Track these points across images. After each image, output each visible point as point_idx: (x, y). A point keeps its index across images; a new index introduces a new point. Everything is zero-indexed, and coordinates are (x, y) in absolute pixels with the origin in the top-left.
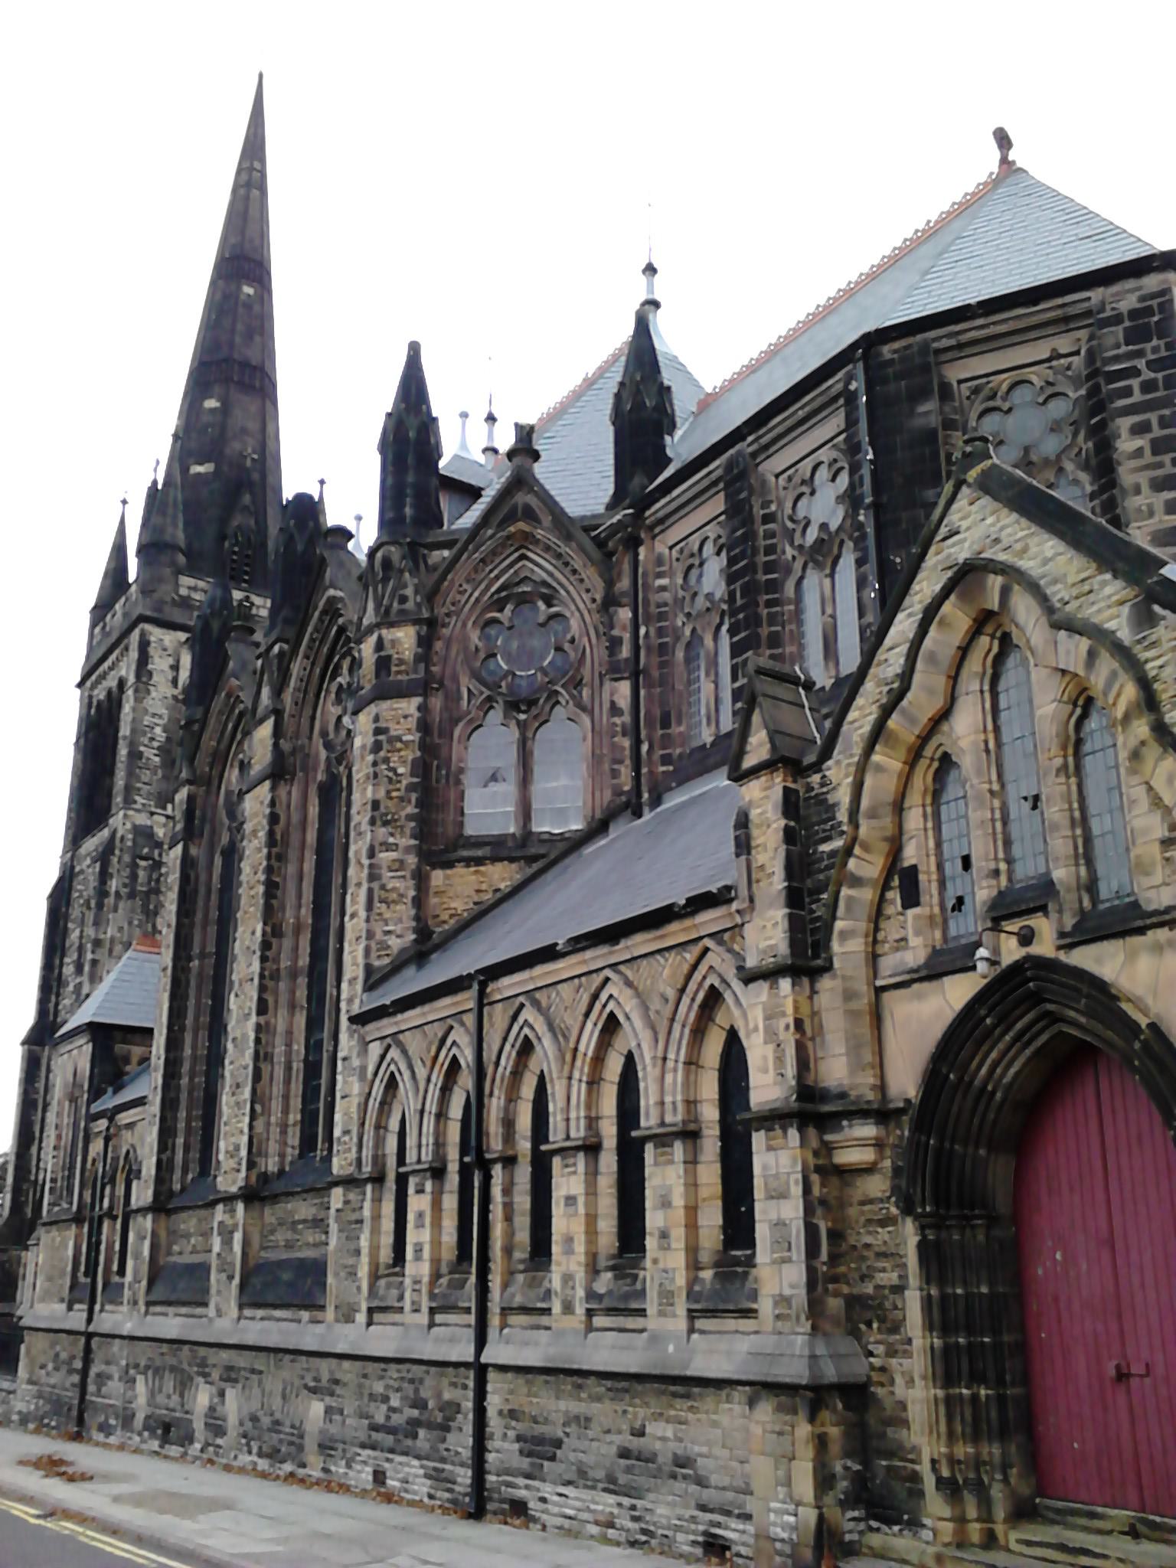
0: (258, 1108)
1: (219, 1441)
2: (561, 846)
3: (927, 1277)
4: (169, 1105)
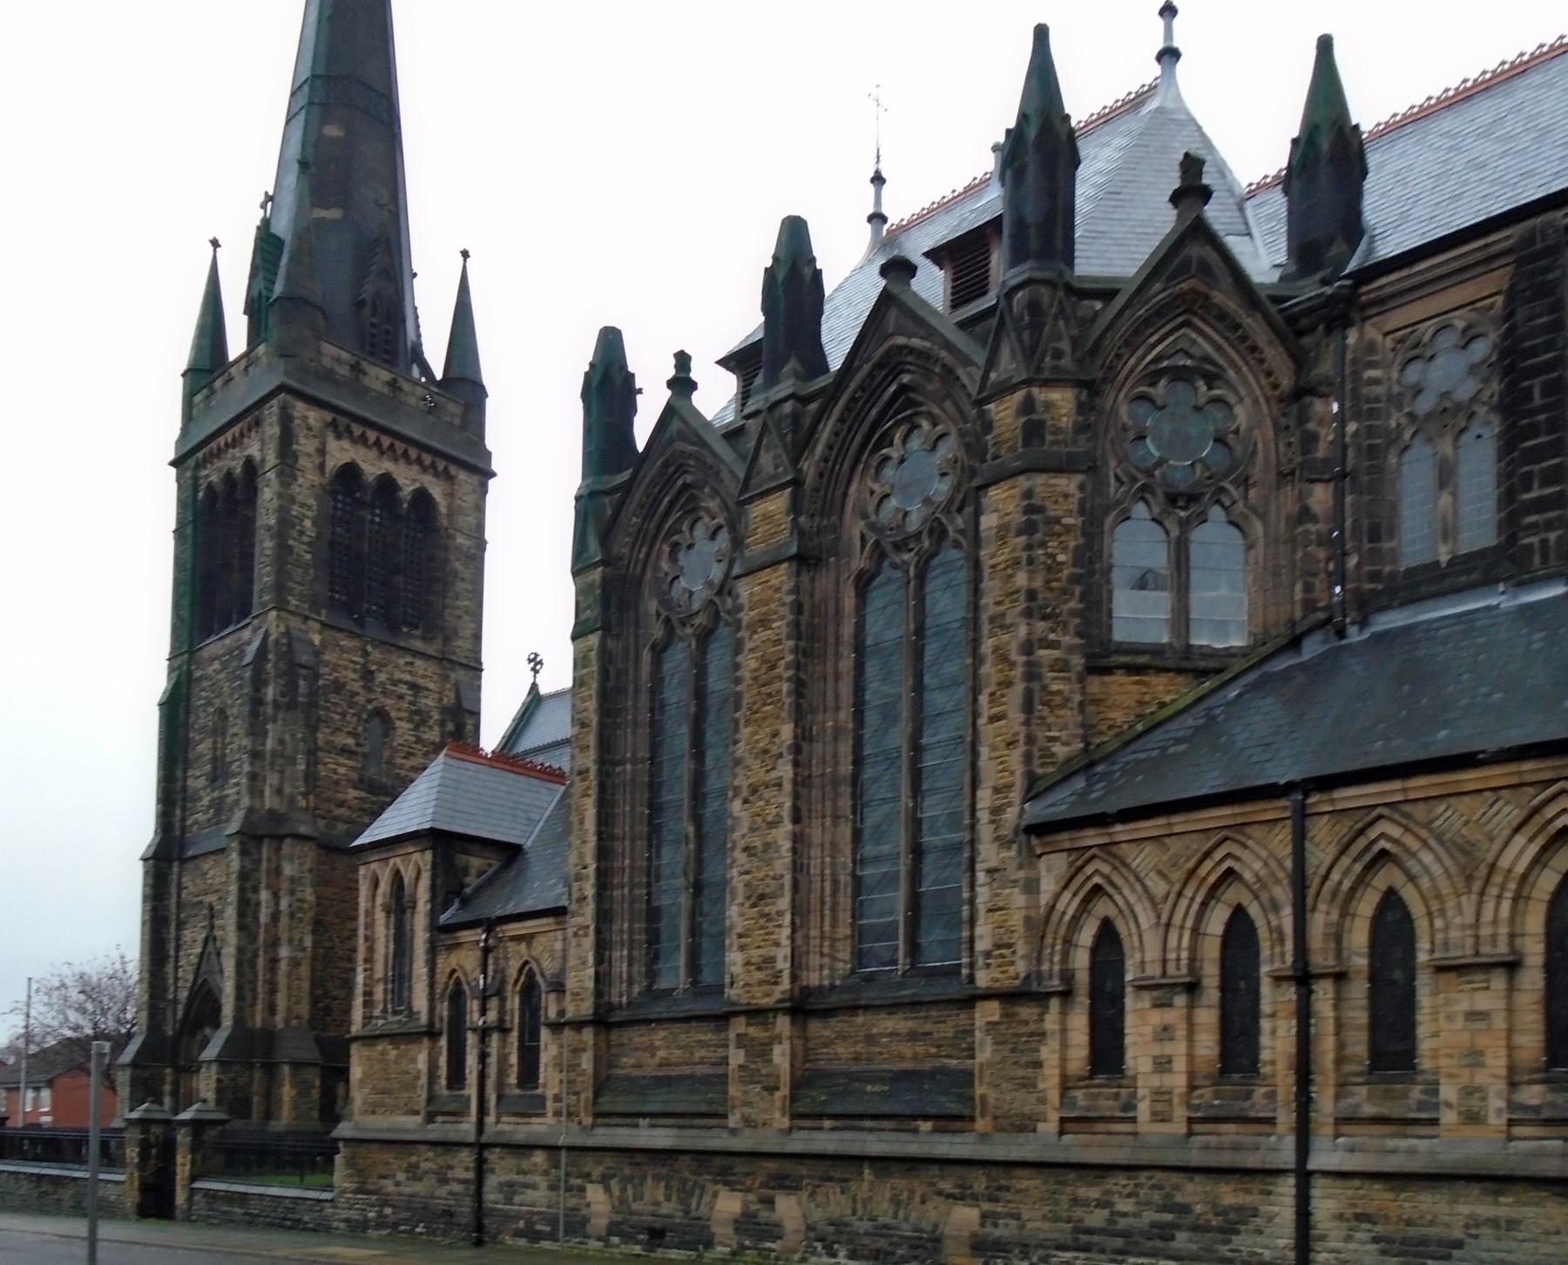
0: (798, 921)
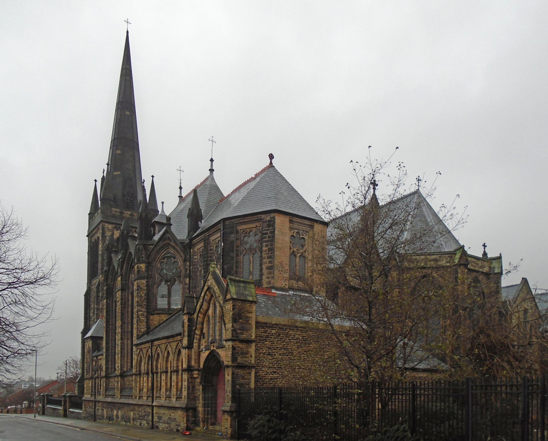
2: (177, 311)
3: (203, 394)
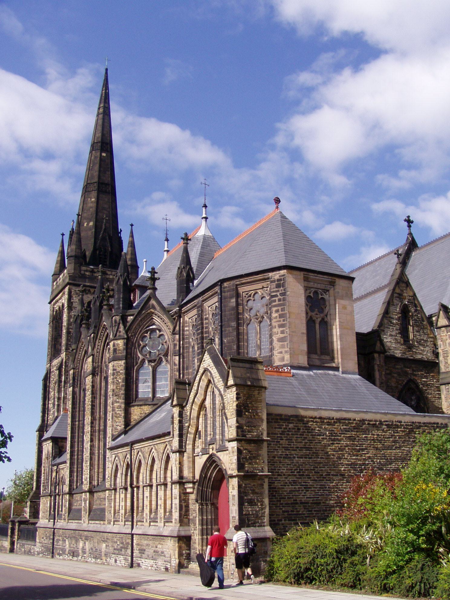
0: (92, 468)
1: (85, 555)
2: (162, 401)
4: (72, 464)
